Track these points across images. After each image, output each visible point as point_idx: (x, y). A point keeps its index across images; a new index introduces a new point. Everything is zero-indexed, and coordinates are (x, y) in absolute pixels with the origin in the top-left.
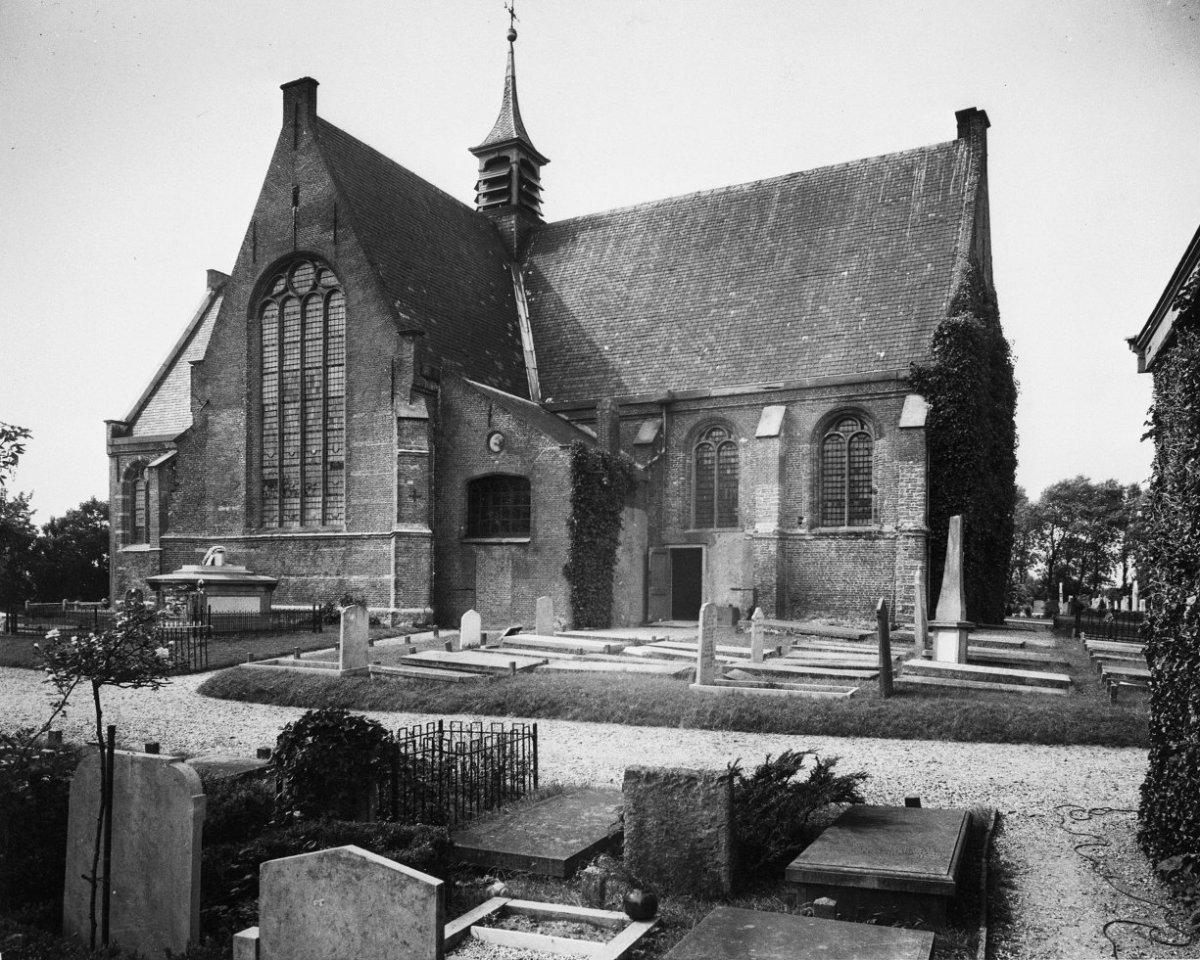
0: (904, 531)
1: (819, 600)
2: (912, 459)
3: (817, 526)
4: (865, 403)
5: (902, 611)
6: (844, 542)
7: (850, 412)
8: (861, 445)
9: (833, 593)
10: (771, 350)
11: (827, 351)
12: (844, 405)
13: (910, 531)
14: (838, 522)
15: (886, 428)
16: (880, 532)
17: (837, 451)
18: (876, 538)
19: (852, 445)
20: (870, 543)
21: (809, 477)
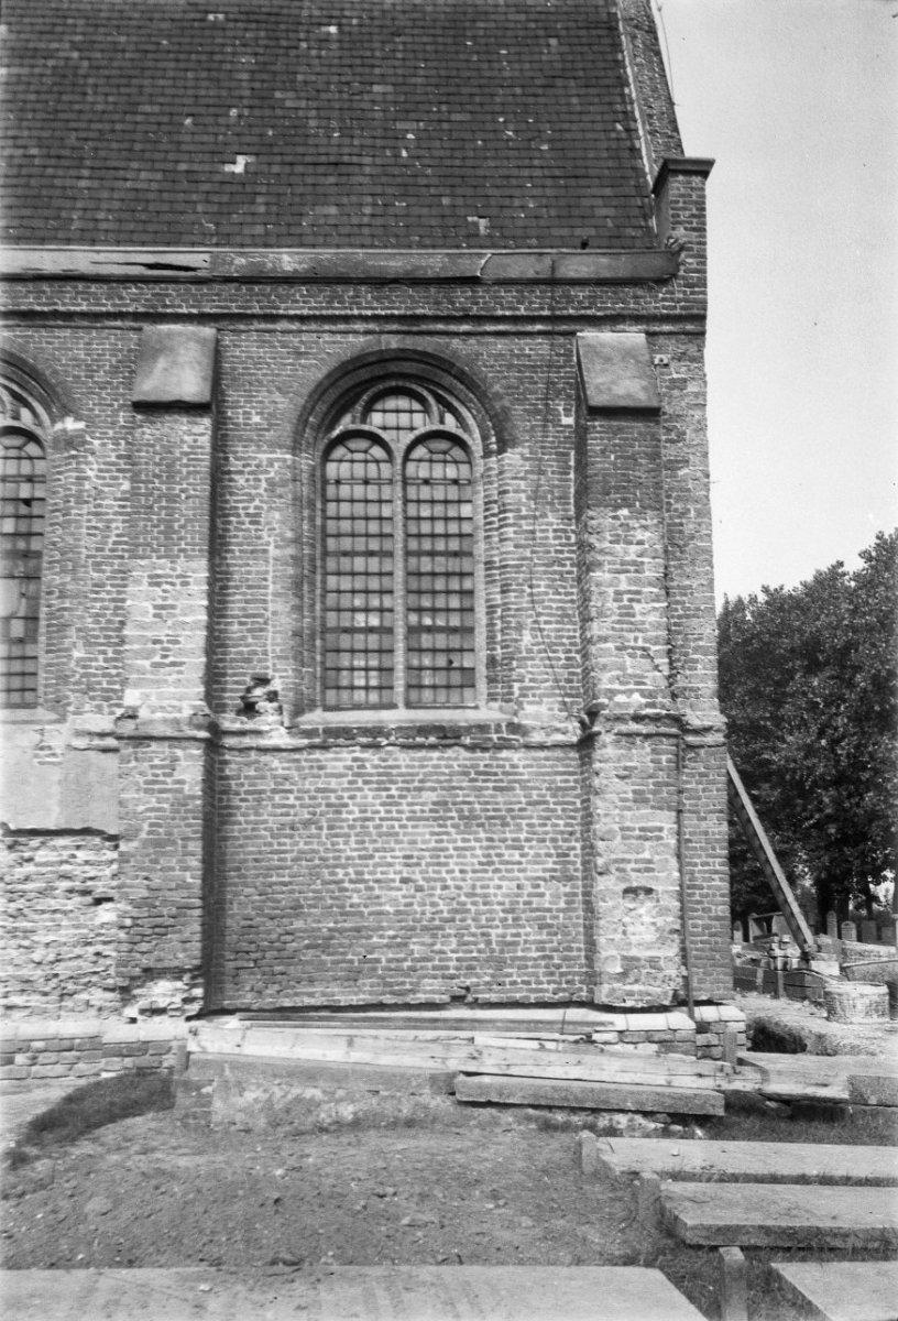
0: (618, 719)
1: (325, 947)
2: (627, 504)
3: (312, 706)
4: (456, 343)
5: (624, 975)
6: (403, 759)
7: (407, 367)
8: (438, 471)
9: (371, 922)
10: (146, 178)
11: (321, 198)
12: (394, 342)
13: (637, 718)
14: (374, 697)
15: (521, 422)
16: (514, 728)
17: (366, 482)
18: (505, 745)
19: (411, 467)
20: (483, 759)
21: (290, 551)
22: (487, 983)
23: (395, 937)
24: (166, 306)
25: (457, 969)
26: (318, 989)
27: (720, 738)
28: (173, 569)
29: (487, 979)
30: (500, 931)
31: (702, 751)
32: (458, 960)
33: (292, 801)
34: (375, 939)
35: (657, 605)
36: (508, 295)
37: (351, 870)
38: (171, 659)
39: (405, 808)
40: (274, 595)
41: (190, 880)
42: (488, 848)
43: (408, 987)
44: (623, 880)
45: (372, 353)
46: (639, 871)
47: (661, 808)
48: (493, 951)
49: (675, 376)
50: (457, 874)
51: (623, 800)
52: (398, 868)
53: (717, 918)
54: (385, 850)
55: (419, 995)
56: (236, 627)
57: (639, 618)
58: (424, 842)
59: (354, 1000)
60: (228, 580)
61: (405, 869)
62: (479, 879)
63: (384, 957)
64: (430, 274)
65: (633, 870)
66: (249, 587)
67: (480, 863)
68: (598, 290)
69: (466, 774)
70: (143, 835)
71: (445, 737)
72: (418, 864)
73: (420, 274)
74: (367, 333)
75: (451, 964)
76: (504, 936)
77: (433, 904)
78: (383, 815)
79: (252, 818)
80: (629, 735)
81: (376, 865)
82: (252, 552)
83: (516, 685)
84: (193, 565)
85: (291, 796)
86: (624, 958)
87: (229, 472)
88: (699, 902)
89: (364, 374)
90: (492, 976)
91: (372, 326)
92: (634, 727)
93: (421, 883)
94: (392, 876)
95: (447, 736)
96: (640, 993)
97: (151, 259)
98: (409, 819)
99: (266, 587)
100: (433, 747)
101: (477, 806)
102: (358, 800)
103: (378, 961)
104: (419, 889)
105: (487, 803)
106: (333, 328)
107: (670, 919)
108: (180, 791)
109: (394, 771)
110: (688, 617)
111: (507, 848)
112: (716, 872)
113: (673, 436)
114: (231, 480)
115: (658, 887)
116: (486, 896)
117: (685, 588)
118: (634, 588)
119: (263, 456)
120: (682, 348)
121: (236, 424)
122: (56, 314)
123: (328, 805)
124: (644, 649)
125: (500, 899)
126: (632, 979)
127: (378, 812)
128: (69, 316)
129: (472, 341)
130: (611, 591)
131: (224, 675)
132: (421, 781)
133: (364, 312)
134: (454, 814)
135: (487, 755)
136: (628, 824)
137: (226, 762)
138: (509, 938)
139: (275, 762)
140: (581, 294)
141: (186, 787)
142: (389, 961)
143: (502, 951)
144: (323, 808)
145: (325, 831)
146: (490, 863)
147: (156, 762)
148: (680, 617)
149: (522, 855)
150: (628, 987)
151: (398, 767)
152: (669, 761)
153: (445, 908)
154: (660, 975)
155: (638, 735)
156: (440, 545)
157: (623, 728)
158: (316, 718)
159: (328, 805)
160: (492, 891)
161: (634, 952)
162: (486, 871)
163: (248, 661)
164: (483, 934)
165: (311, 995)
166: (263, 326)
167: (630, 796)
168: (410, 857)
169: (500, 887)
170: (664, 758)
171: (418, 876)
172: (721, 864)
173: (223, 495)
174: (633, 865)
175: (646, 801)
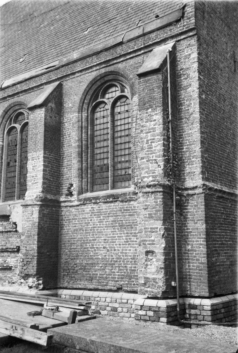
4: (120, 65)
5: (145, 284)
6: (104, 206)
7: (110, 77)
9: (96, 261)
12: (103, 71)
13: (149, 186)
20: (126, 205)
22: (126, 284)
23: (101, 267)
24: (50, 78)
25: (118, 278)
26: (82, 283)
27: (201, 190)
28: (36, 155)
29: (127, 282)
30: (130, 266)
31: (195, 196)
32: (118, 275)
33: (77, 222)
34: (96, 267)
35: (159, 143)
36: (131, 44)
37: (90, 244)
38: (36, 181)
39: (104, 223)
40: (74, 158)
41: (34, 248)
42: (127, 236)
43: (105, 284)
44: (145, 248)
45: (98, 76)
46: (150, 244)
47: (157, 220)
48: (128, 273)
49: (186, 54)
50: (118, 245)
51: (145, 217)
52: (102, 243)
53: (202, 263)
54: (99, 237)
55: (108, 287)
56: (65, 170)
57: (154, 148)
58: (110, 235)
59: (91, 287)
60: (64, 155)
61: (104, 244)
62: (124, 247)
63: (98, 273)
64: (109, 46)
65: (148, 244)
66: (68, 157)
67: (125, 242)
68: (158, 32)
69: (121, 211)
70: (26, 234)
71: (115, 198)
72: (108, 242)
73: (107, 47)
74: (96, 70)
75: (117, 276)
76: (131, 267)
77: (112, 256)
78: (98, 226)
79: (68, 228)
80: (146, 193)
81: (97, 243)
82: (69, 146)
83: (136, 178)
84: (40, 153)
85: (77, 220)
86: (145, 278)
87: (64, 123)
88: (195, 257)
89: (99, 83)
90: (128, 281)
91: (98, 68)
92: (148, 190)
93: (108, 248)
94: (101, 246)
95: (115, 198)
96: (150, 292)
97: (46, 67)
98: (105, 227)
99: (72, 156)
100: (111, 202)
101: (124, 222)
102: (92, 221)
103: (97, 274)
104: (108, 251)
105: (127, 220)
106: (88, 71)
107: (160, 263)
108: (33, 221)
109: (102, 211)
110: (190, 145)
111: (132, 236)
112: (201, 244)
113: (186, 76)
114: (64, 125)
115: (156, 251)
116: (126, 253)
117: (189, 134)
118: (152, 138)
119: (71, 116)
120: (189, 43)
121: (66, 108)
122: (30, 89)
123: (85, 223)
124: (155, 160)
125: (130, 254)
126: (147, 286)
127: (97, 225)
128: (33, 88)
129: (124, 63)
130: (145, 140)
131: (63, 184)
132: (109, 214)
133: (94, 64)
134: (117, 225)
135: (127, 204)
136: (147, 227)
137: (62, 211)
138: (133, 268)
139: (73, 210)
140: (153, 35)
141: (35, 219)
142: (100, 274)
143: (131, 273)
144: (84, 224)
145: (84, 232)
146: (127, 242)
147: (29, 212)
148: (187, 145)
149: (137, 239)
150: (146, 289)
151: (102, 209)
152: (160, 202)
153: (115, 257)
154: (157, 285)
155: (149, 192)
156: (123, 134)
157: (144, 190)
158: (84, 196)
159: (85, 223)
160: (128, 251)
161: (148, 276)
162: (126, 244)
163: (68, 179)
164: (125, 267)
165: (80, 284)
166: (73, 77)
167: (147, 216)
168: (105, 240)
169: (130, 250)
170: (158, 200)
171: (108, 246)
172: (203, 241)
173: (62, 130)
174: (148, 242)
175: (152, 217)
